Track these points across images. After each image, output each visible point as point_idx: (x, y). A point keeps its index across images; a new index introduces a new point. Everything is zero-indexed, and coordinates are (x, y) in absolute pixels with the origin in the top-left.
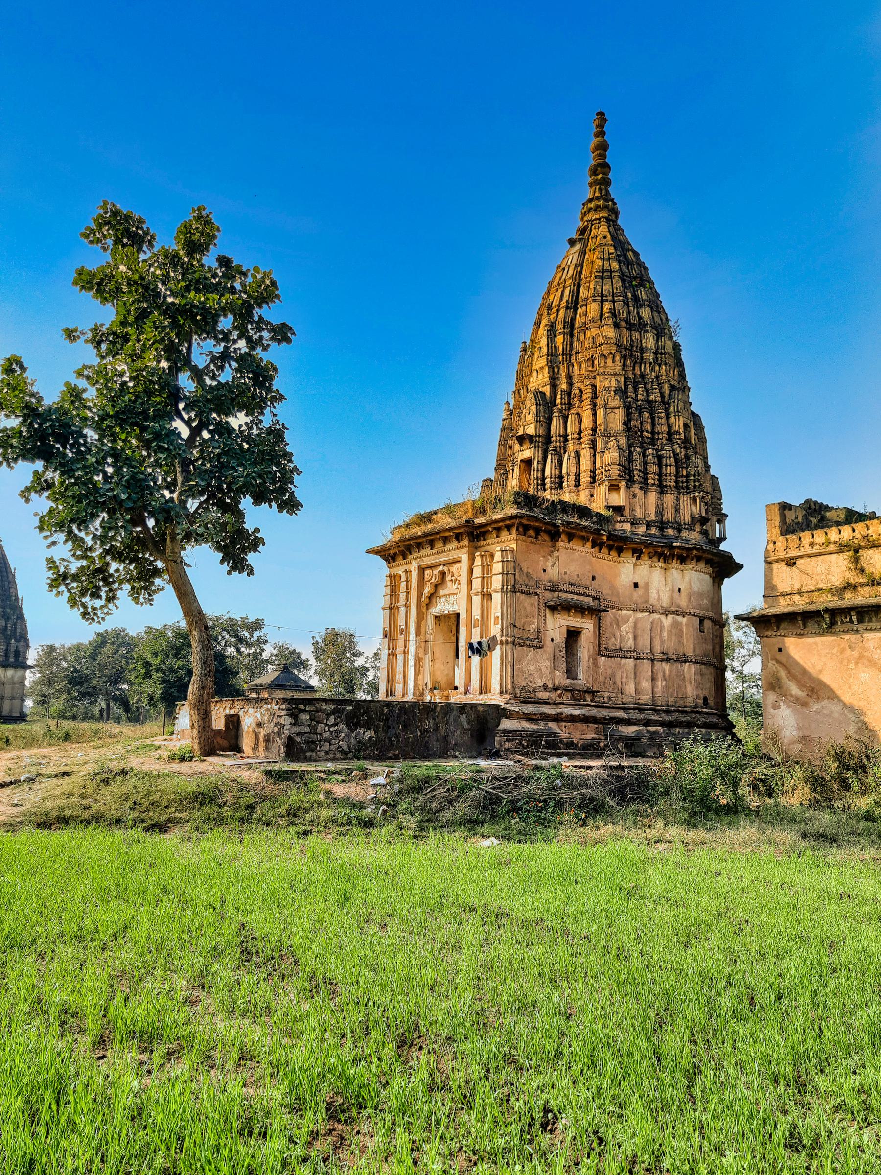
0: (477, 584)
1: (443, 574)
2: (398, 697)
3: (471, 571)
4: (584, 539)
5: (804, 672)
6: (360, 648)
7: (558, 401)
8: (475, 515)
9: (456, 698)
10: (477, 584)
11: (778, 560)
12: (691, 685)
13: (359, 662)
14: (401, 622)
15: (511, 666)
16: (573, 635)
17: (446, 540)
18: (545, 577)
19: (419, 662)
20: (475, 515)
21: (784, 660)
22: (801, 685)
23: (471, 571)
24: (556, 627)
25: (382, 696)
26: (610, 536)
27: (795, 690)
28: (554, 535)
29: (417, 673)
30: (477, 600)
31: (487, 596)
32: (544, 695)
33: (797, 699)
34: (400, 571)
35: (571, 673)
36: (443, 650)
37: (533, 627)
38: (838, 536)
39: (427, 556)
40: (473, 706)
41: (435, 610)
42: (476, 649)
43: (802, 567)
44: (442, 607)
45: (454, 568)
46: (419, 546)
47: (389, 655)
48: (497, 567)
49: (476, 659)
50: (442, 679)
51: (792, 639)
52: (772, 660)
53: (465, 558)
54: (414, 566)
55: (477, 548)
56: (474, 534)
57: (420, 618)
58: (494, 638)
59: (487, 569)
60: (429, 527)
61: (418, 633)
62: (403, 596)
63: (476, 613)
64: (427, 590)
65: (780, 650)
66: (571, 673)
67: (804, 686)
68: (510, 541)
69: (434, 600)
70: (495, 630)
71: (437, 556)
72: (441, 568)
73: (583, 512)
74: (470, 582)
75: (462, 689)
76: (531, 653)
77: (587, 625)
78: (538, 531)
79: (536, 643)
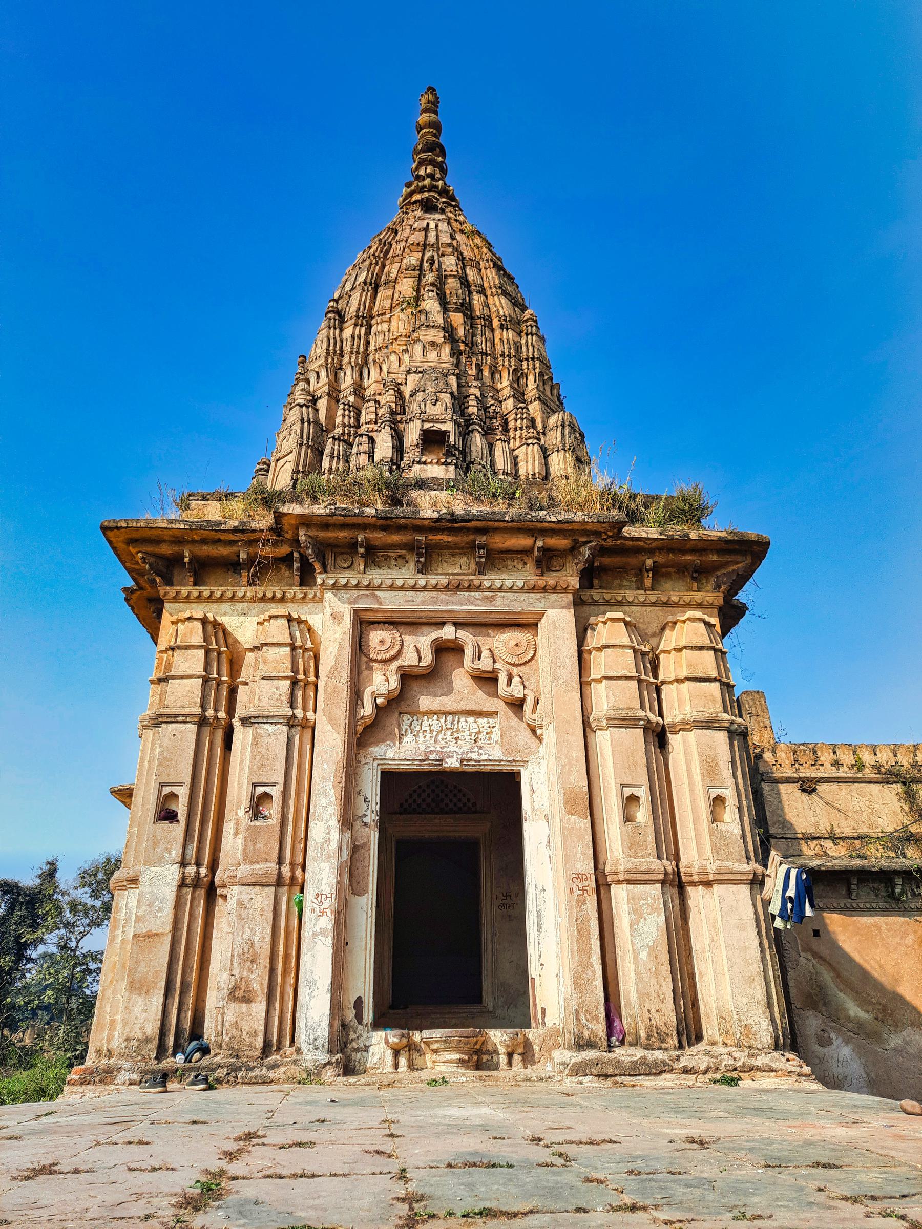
5: (865, 975)
7: (338, 420)
11: (788, 780)
17: (494, 559)
21: (824, 951)
22: (863, 1002)
27: (854, 1010)
33: (860, 1024)
38: (874, 758)
39: (398, 587)
43: (828, 798)
47: (182, 885)
51: (835, 916)
52: (804, 950)
64: (381, 683)
65: (816, 933)
67: (870, 1003)
69: (391, 720)
71: (443, 596)
72: (448, 632)
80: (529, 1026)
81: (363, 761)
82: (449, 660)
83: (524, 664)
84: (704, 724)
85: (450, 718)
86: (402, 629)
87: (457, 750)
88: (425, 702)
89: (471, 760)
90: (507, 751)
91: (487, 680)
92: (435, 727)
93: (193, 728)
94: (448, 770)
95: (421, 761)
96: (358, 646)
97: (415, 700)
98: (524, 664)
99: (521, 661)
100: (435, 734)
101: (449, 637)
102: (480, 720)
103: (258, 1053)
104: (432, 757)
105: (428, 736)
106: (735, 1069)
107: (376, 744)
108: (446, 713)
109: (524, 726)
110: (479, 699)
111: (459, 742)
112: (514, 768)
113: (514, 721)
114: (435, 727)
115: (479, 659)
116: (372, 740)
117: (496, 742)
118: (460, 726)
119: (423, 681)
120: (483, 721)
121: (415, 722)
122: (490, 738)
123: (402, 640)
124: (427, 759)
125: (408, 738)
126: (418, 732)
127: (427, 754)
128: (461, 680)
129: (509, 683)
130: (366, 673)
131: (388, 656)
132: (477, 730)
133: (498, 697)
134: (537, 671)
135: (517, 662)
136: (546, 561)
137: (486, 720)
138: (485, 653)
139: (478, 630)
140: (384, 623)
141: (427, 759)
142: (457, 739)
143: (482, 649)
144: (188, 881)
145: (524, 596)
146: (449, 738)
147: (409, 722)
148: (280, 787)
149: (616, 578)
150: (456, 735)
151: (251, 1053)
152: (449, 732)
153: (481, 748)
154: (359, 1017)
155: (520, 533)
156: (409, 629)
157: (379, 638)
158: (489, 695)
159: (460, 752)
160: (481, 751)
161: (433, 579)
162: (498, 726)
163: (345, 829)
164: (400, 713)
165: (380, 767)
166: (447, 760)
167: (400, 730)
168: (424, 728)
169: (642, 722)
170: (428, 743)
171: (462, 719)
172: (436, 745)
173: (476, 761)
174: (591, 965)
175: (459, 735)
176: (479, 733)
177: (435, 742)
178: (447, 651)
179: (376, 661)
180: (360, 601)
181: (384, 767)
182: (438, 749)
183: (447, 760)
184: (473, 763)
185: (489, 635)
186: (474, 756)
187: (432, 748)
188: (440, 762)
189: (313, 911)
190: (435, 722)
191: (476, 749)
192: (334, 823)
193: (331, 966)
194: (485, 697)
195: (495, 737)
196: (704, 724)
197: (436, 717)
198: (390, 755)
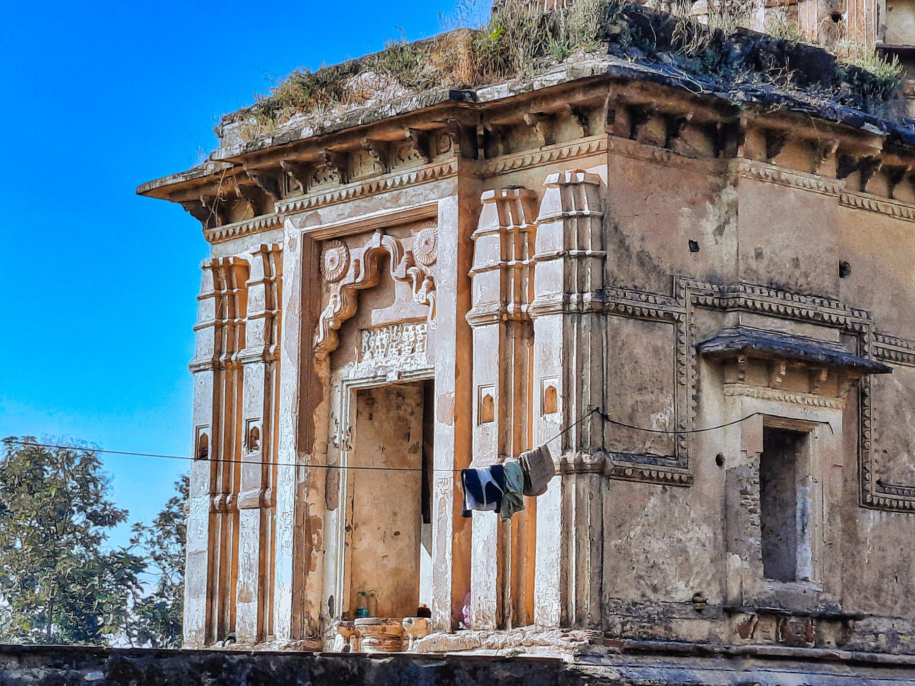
0: (486, 289)
1: (380, 259)
2: (245, 636)
3: (467, 250)
4: (814, 150)
6: (114, 496)
8: (480, 74)
9: (421, 641)
10: (486, 289)
12: (598, 221)
13: (114, 541)
14: (252, 407)
15: (594, 538)
16: (782, 443)
17: (389, 154)
18: (696, 267)
19: (307, 530)
20: (480, 74)
23: (467, 250)
24: (731, 418)
25: (192, 637)
26: (896, 141)
28: (724, 137)
29: (303, 566)
30: (486, 338)
31: (518, 327)
32: (693, 630)
34: (245, 250)
35: (776, 560)
36: (377, 494)
37: (660, 420)
39: (332, 205)
40: (481, 668)
41: (357, 371)
42: (487, 490)
44: (378, 360)
45: (416, 240)
46: (307, 173)
47: (213, 511)
48: (550, 237)
49: (485, 521)
50: (380, 584)
53: (448, 207)
54: (290, 236)
55: (486, 178)
56: (476, 135)
57: (311, 394)
58: (542, 455)
59: (516, 240)
60: (336, 114)
61: (304, 443)
62: (255, 329)
63: (486, 377)
64: (333, 307)
66: (776, 560)
68: (587, 156)
69: (352, 340)
70: (545, 431)
71: (363, 203)
72: (374, 242)
73: (811, 65)
74: (465, 284)
75: (442, 614)
76: (654, 500)
77: (825, 416)
78: (674, 125)
79: (672, 470)
84: (543, 310)
93: (210, 373)
103: (254, 640)
106: (521, 645)
116: (340, 362)
136: (427, 145)
140: (335, 239)
144: (217, 508)
145: (420, 189)
148: (261, 422)
149: (524, 134)
151: (250, 640)
154: (331, 612)
155: (391, 125)
160: (413, 362)
161: (354, 186)
163: (302, 453)
169: (495, 318)
174: (445, 561)
180: (308, 223)
186: (407, 368)
189: (281, 528)
192: (292, 450)
193: (291, 571)
196: (543, 310)
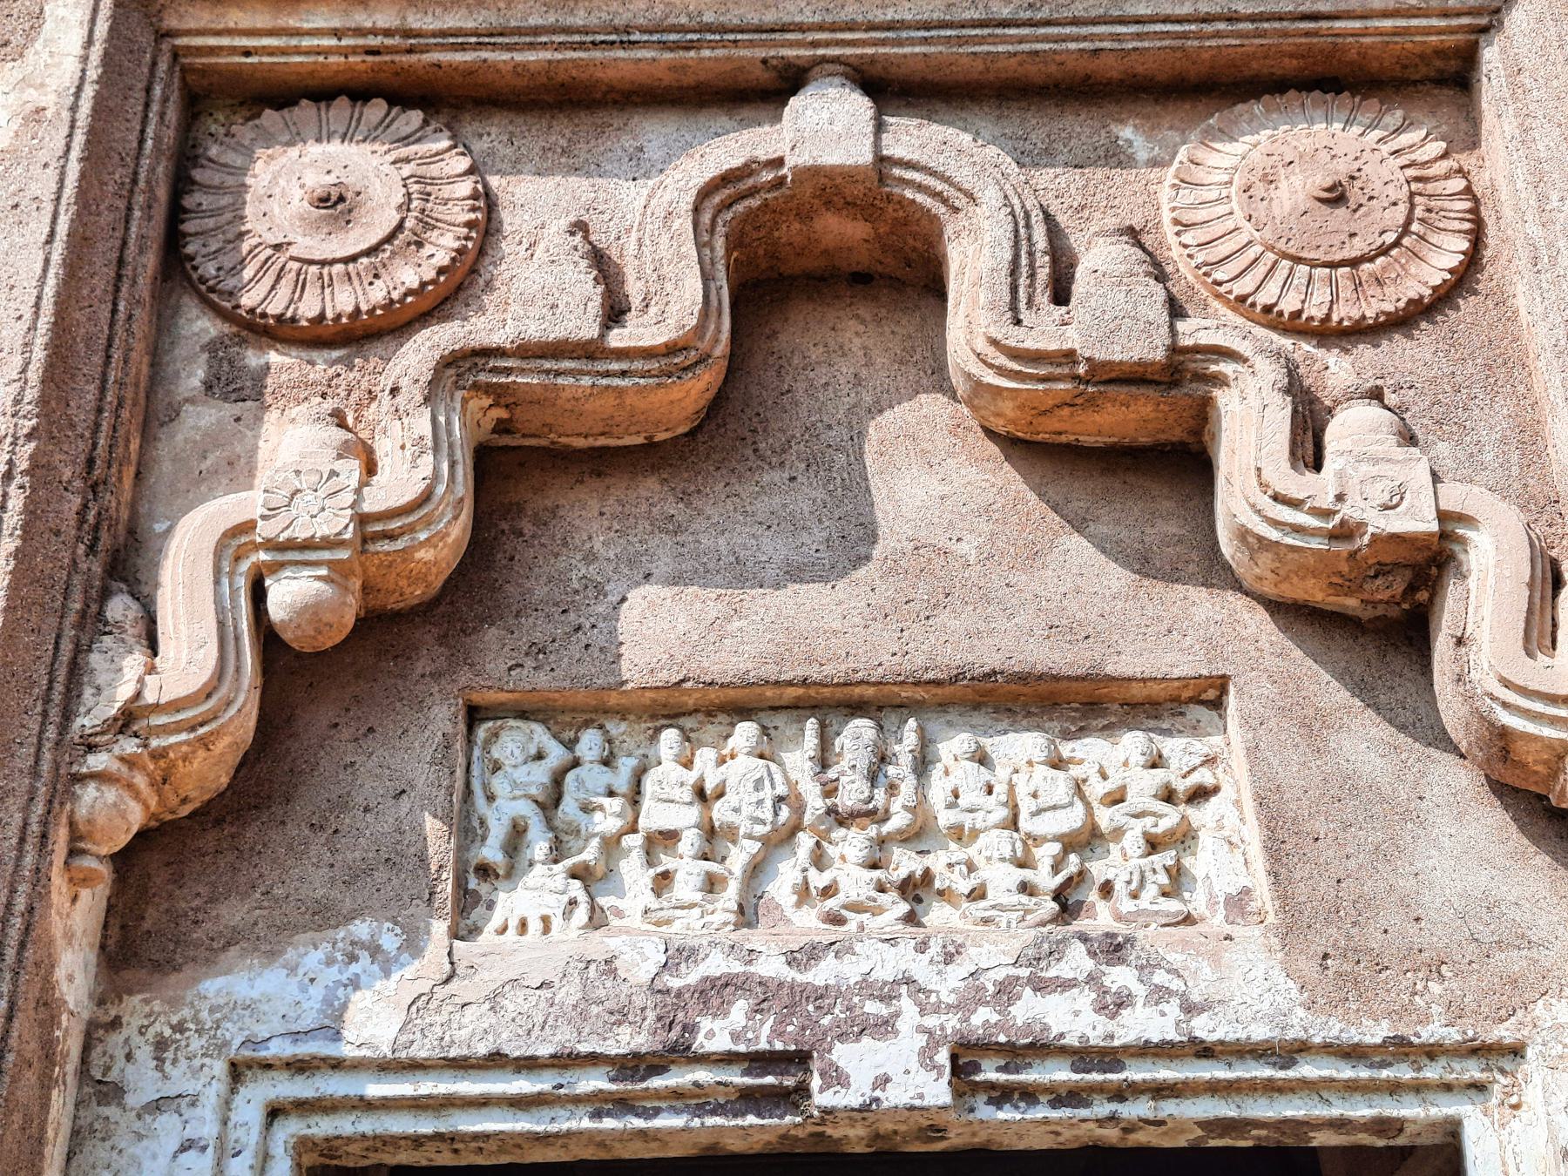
64: (315, 474)
72: (826, 128)
80: (737, 828)
81: (143, 1082)
82: (835, 351)
83: (1405, 320)
85: (857, 734)
86: (491, 136)
87: (921, 969)
88: (660, 627)
89: (1042, 1049)
90: (1345, 969)
91: (1130, 450)
92: (746, 798)
94: (854, 1138)
95: (633, 1065)
96: (146, 228)
97: (585, 614)
98: (1405, 320)
99: (1374, 307)
100: (738, 857)
101: (833, 157)
102: (1090, 751)
104: (715, 1035)
105: (687, 869)
107: (267, 942)
108: (830, 703)
109: (1455, 781)
110: (1077, 592)
111: (938, 915)
112: (1409, 1110)
113: (1364, 742)
114: (746, 798)
115: (1061, 295)
117: (1238, 903)
118: (938, 791)
119: (650, 486)
120: (1113, 755)
121: (591, 776)
122: (1177, 880)
123: (487, 201)
124: (680, 1053)
125: (538, 891)
126: (611, 845)
127: (677, 1010)
128: (929, 473)
129: (1308, 446)
130: (203, 418)
131: (377, 294)
132: (1072, 819)
133: (1215, 572)
134: (1506, 365)
135: (1346, 312)
137: (1133, 743)
138: (1098, 258)
139: (1039, 126)
140: (360, 93)
141: (680, 1053)
142: (915, 889)
143: (1076, 240)
146: (854, 882)
147: (540, 775)
150: (905, 863)
152: (851, 844)
153: (1113, 949)
156: (535, 136)
157: (317, 181)
158: (1144, 564)
159: (948, 983)
160: (1120, 977)
162: (1236, 781)
164: (474, 715)
165: (290, 1129)
166: (842, 1054)
167: (467, 829)
168: (654, 816)
170: (686, 927)
171: (954, 745)
172: (754, 939)
173: (1084, 1056)
175: (937, 862)
176: (1087, 840)
177: (746, 915)
178: (820, 274)
179: (282, 332)
181: (324, 1127)
182: (771, 967)
183: (842, 1054)
184: (1060, 1073)
185: (1116, 157)
186: (1070, 1017)
187: (717, 964)
188: (782, 1071)
190: (744, 768)
191: (1077, 961)
194: (1118, 577)
195: (1228, 852)
197: (745, 733)
198: (373, 1023)
